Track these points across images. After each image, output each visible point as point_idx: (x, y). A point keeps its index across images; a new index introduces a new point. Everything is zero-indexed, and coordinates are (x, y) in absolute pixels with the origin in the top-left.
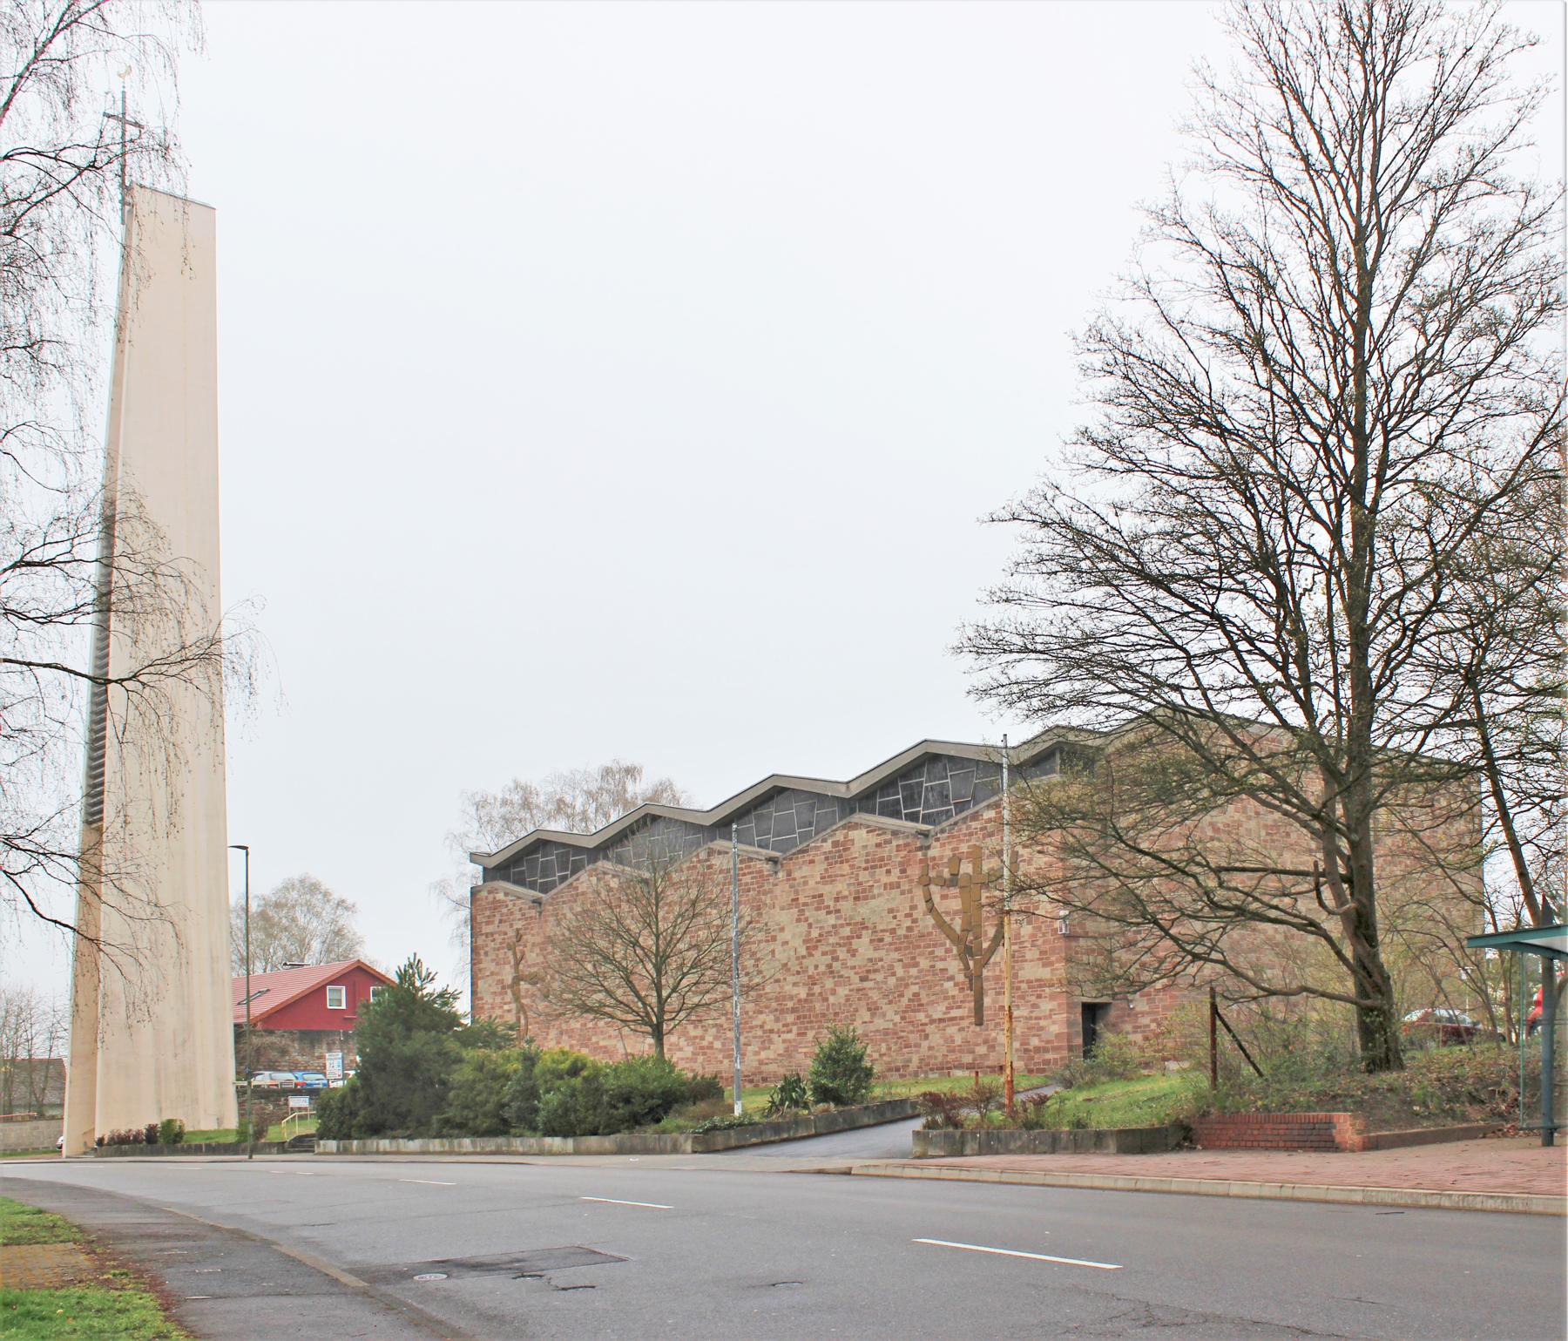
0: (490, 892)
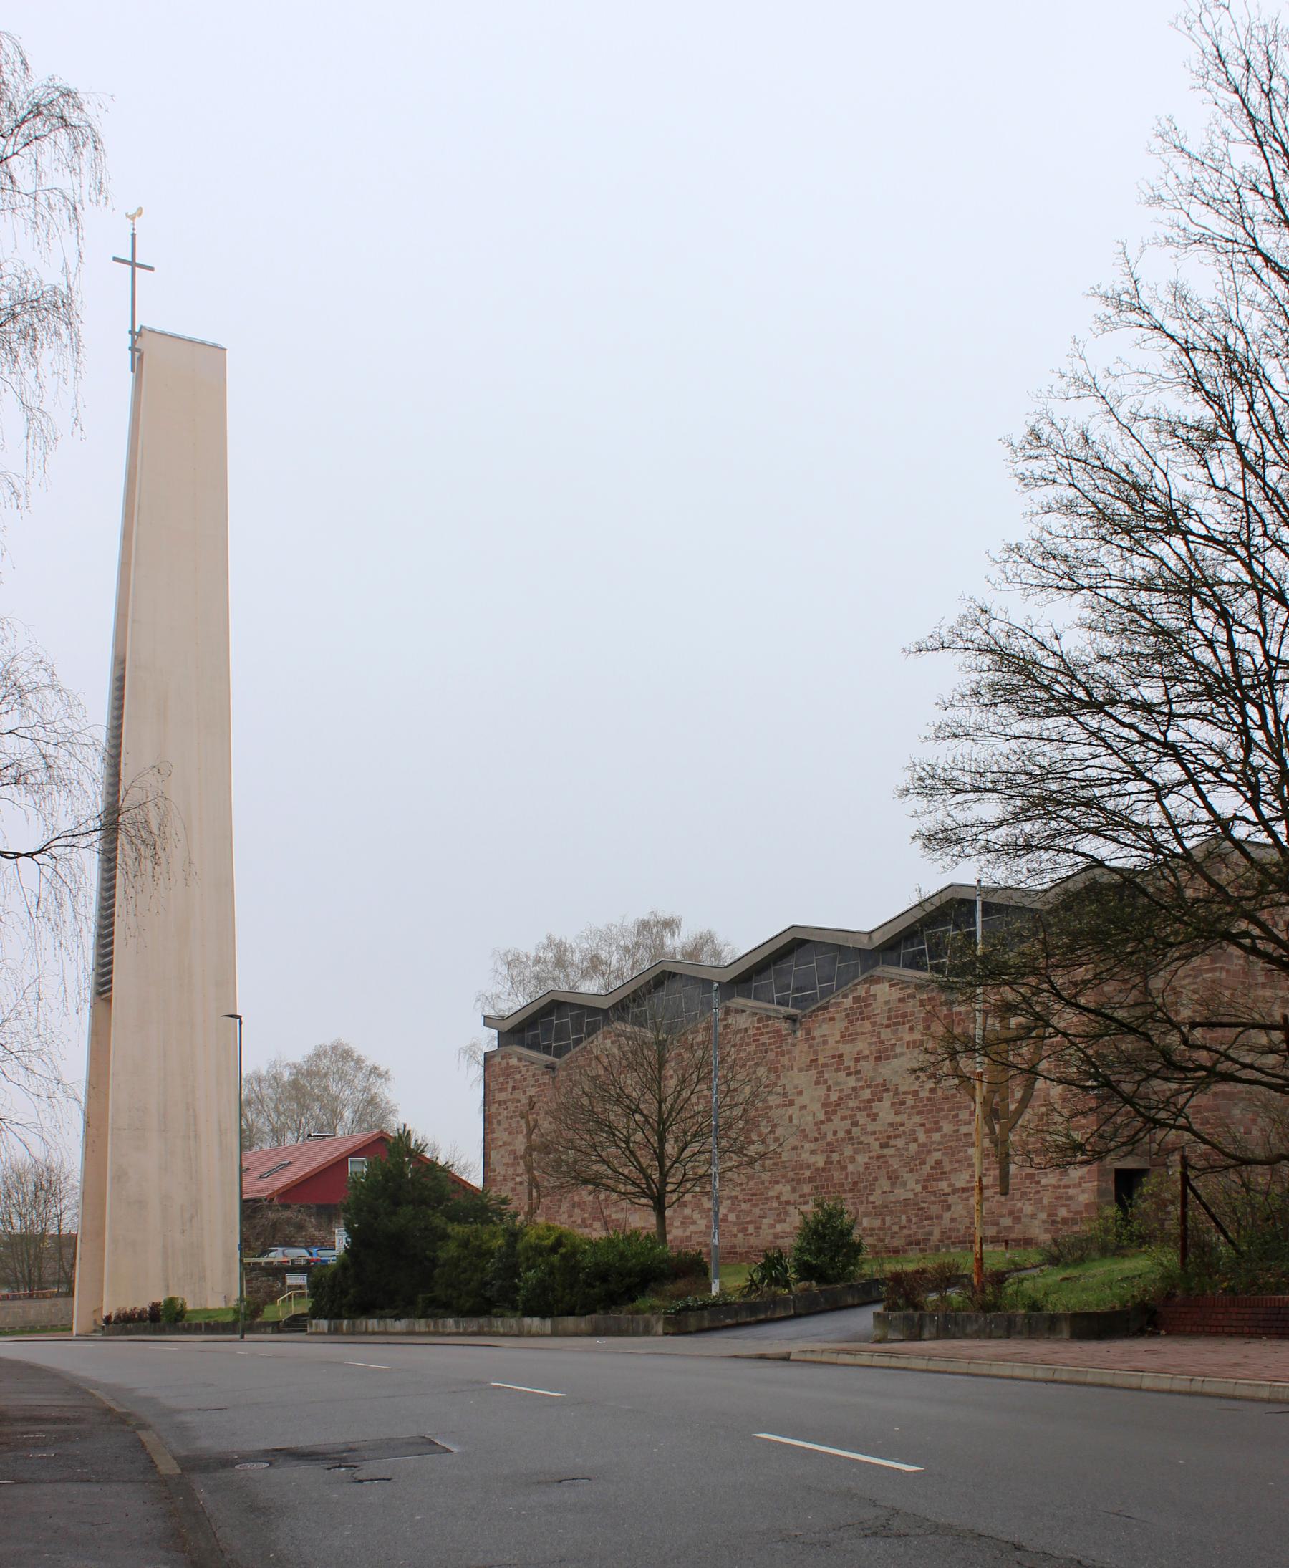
0: (503, 1058)
